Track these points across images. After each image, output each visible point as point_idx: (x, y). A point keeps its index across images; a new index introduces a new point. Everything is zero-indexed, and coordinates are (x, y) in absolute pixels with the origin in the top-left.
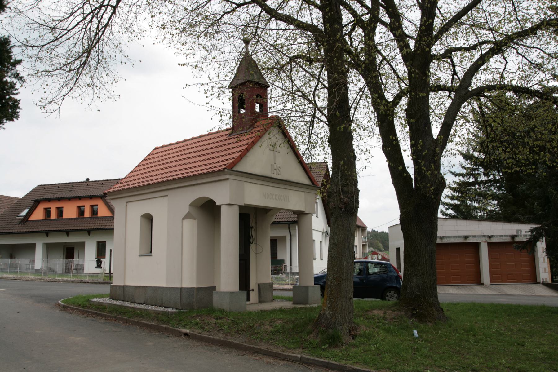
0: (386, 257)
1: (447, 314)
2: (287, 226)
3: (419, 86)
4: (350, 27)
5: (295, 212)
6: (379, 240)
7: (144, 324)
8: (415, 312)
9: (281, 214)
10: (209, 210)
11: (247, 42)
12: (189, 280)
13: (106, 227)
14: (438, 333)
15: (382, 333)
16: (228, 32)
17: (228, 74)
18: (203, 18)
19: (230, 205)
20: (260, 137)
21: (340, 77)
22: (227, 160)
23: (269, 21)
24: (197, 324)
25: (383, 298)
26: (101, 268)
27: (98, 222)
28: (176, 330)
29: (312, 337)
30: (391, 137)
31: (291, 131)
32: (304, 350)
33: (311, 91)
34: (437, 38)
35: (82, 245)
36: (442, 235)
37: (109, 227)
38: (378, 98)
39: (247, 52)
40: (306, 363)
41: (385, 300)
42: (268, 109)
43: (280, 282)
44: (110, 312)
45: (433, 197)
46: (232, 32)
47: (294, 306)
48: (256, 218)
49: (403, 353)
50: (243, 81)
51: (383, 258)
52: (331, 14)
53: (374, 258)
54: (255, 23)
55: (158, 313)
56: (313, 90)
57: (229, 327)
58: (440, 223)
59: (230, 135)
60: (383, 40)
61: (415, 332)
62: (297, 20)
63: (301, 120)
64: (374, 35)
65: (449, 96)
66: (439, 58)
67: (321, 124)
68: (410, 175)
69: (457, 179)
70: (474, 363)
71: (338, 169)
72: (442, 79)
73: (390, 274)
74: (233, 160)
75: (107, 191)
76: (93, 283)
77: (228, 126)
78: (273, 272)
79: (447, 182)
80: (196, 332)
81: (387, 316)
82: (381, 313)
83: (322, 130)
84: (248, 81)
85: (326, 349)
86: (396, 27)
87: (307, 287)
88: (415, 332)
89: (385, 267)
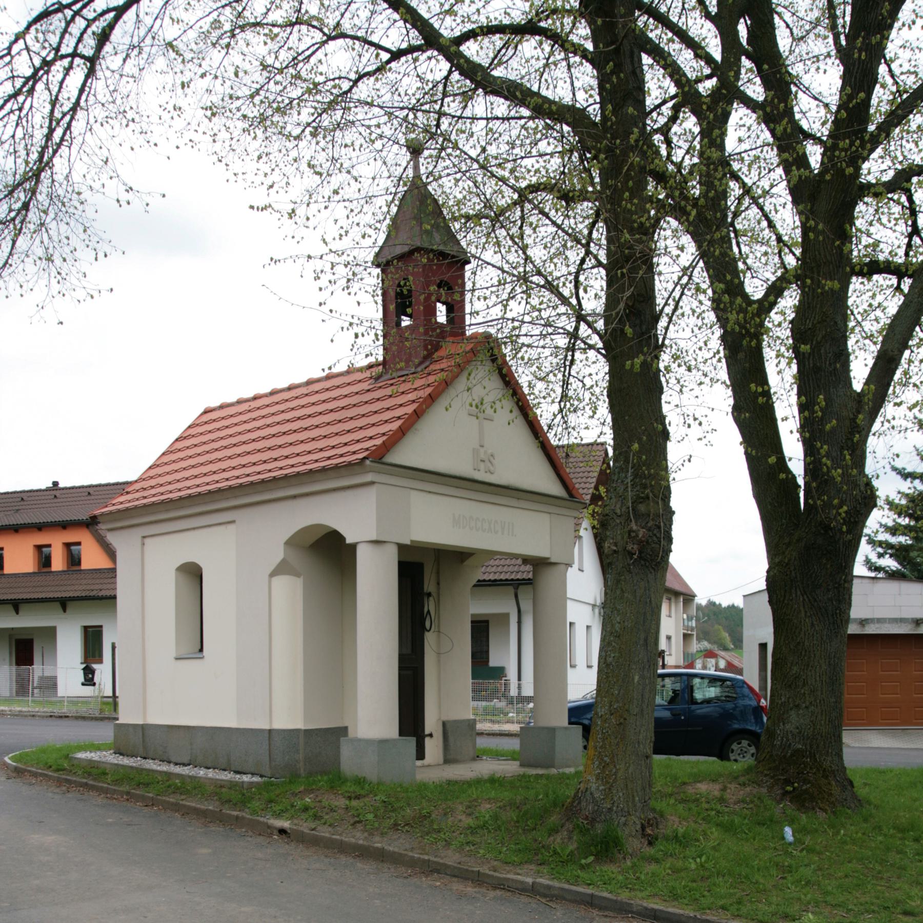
0: (736, 663)
1: (862, 792)
2: (511, 590)
3: (826, 262)
4: (666, 110)
5: (526, 560)
6: (721, 623)
7: (189, 807)
8: (789, 788)
9: (497, 562)
10: (330, 553)
11: (415, 150)
12: (287, 713)
13: (100, 594)
14: (838, 833)
15: (715, 834)
16: (369, 127)
17: (370, 231)
18: (309, 91)
19: (377, 542)
20: (446, 384)
21: (636, 241)
22: (371, 438)
23: (467, 97)
24: (306, 809)
25: (723, 755)
26: (94, 684)
27: (84, 582)
28: (259, 822)
29: (559, 840)
30: (753, 386)
31: (520, 370)
32: (540, 868)
33: (570, 274)
34: (875, 141)
35: (51, 633)
36: (863, 615)
37: (108, 593)
38: (724, 292)
39: (417, 176)
40: (545, 896)
41: (728, 759)
42: (467, 317)
43: (494, 718)
44: (116, 782)
45: (844, 528)
46: (378, 126)
47: (522, 771)
48: (438, 573)
49: (757, 876)
50: (406, 249)
51: (730, 667)
52: (618, 77)
53: (709, 665)
54: (435, 102)
55: (220, 785)
56: (574, 270)
57: (376, 816)
58: (857, 589)
59: (378, 378)
60: (745, 146)
61: (788, 832)
62: (538, 94)
63: (542, 343)
64: (723, 134)
65: (898, 288)
66: (880, 191)
67: (592, 354)
68: (794, 477)
69: (906, 486)
70: (910, 897)
71: (627, 461)
72: (882, 246)
73: (741, 702)
74: (385, 438)
75: (97, 512)
76: (77, 718)
77: (372, 360)
78: (478, 694)
79: (881, 493)
80: (305, 827)
81: (727, 796)
82: (714, 789)
83: (594, 369)
84: (418, 250)
85: (588, 865)
86: (777, 112)
87: (552, 731)
88: (788, 832)
89: (732, 687)
